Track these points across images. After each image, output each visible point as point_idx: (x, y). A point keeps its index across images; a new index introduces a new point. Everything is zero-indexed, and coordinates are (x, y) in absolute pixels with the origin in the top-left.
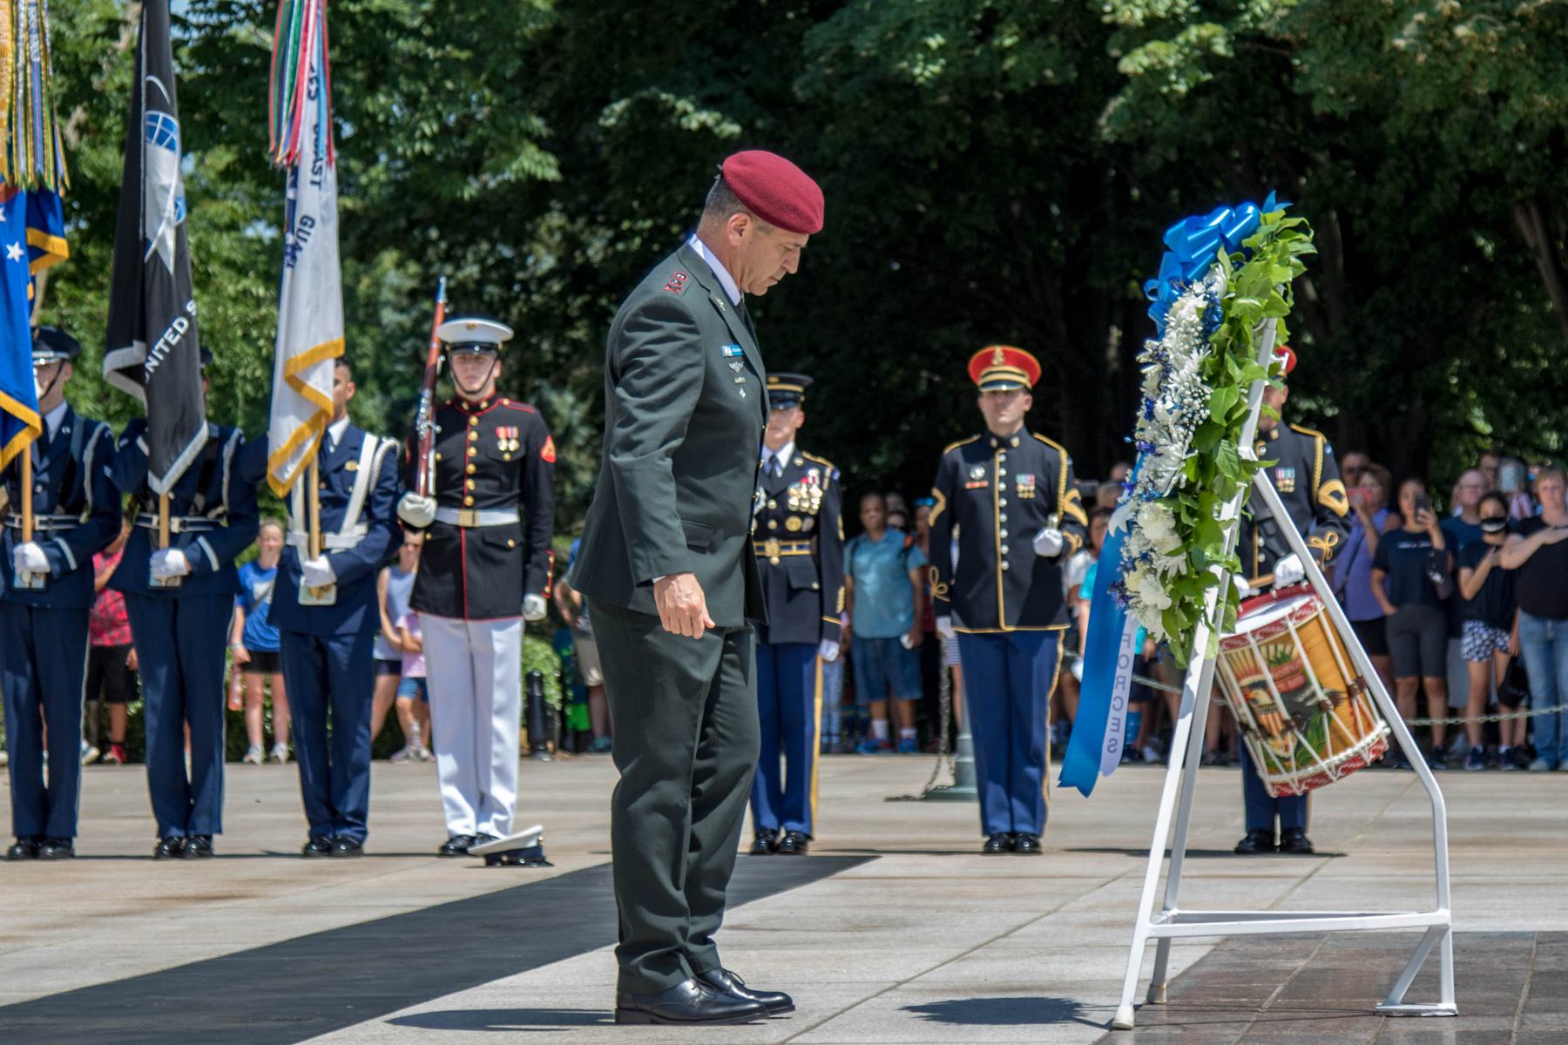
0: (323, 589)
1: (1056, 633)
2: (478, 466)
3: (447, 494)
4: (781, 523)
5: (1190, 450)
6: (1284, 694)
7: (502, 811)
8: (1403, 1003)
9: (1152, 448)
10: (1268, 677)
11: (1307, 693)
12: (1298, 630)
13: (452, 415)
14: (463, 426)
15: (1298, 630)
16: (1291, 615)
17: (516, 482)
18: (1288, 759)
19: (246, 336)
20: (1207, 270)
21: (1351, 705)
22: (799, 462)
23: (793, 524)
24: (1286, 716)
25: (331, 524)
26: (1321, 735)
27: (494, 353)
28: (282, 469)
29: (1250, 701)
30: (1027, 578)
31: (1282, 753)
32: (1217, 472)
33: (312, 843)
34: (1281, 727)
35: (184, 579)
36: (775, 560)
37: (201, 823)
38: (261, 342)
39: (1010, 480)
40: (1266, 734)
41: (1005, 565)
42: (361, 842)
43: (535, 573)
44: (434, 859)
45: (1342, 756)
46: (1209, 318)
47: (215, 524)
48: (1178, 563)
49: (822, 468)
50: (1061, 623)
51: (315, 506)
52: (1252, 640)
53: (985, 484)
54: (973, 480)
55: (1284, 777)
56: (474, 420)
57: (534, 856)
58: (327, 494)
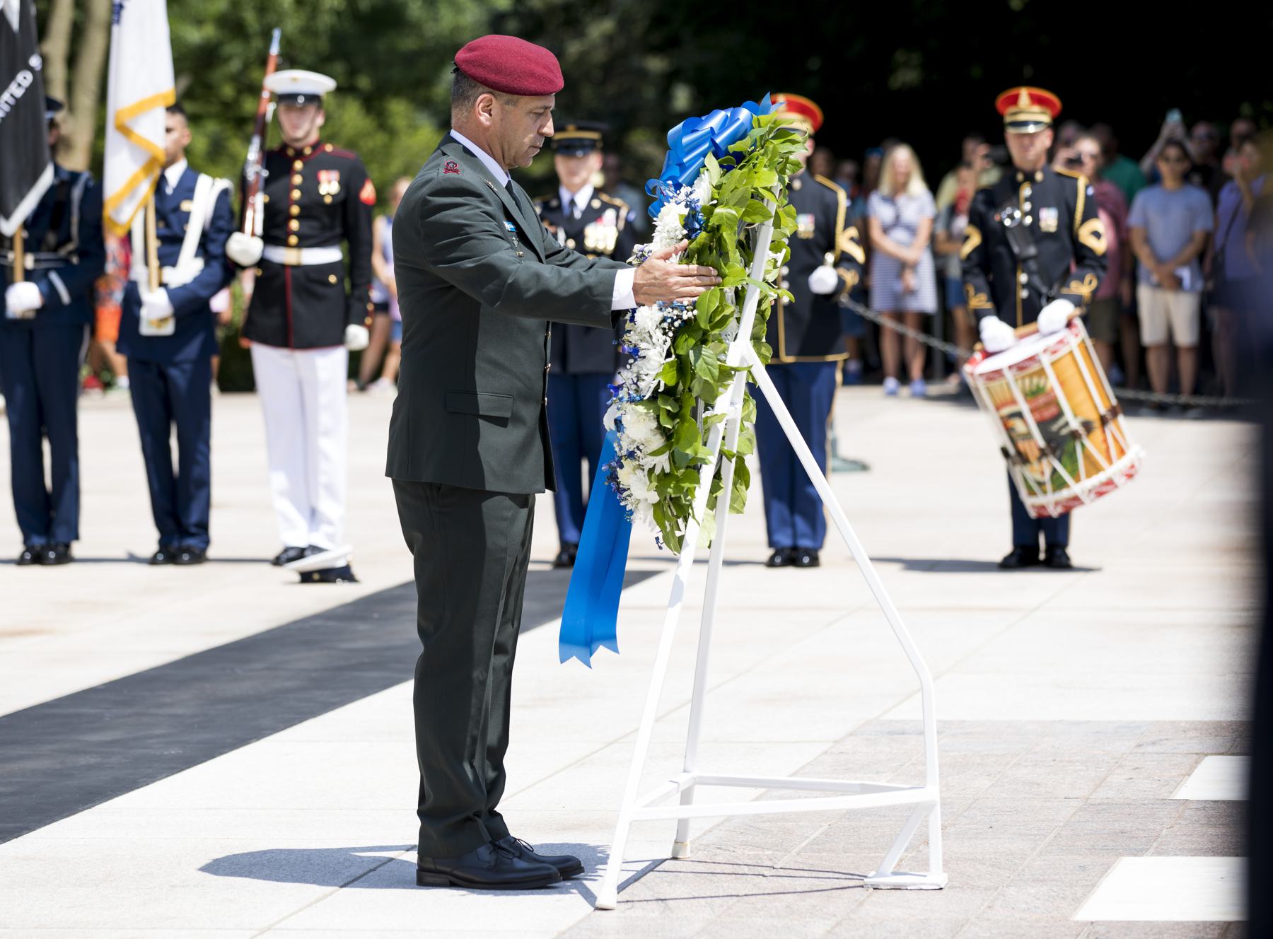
0: (163, 321)
1: (834, 363)
2: (302, 207)
3: (274, 233)
5: (668, 355)
7: (330, 523)
8: (895, 874)
9: (635, 351)
10: (1024, 407)
11: (1061, 422)
13: (279, 161)
14: (290, 171)
15: (1053, 364)
17: (338, 222)
20: (697, 174)
22: (596, 204)
24: (1041, 443)
25: (169, 257)
26: (1073, 455)
28: (118, 210)
30: (806, 313)
31: (1039, 477)
32: (694, 375)
33: (160, 552)
35: (39, 312)
37: (61, 533)
40: (1023, 459)
42: (204, 550)
43: (356, 306)
46: (690, 223)
47: (66, 261)
48: (663, 462)
49: (617, 209)
50: (839, 352)
51: (154, 244)
52: (1009, 375)
55: (1040, 500)
56: (298, 165)
57: (345, 574)
58: (165, 232)
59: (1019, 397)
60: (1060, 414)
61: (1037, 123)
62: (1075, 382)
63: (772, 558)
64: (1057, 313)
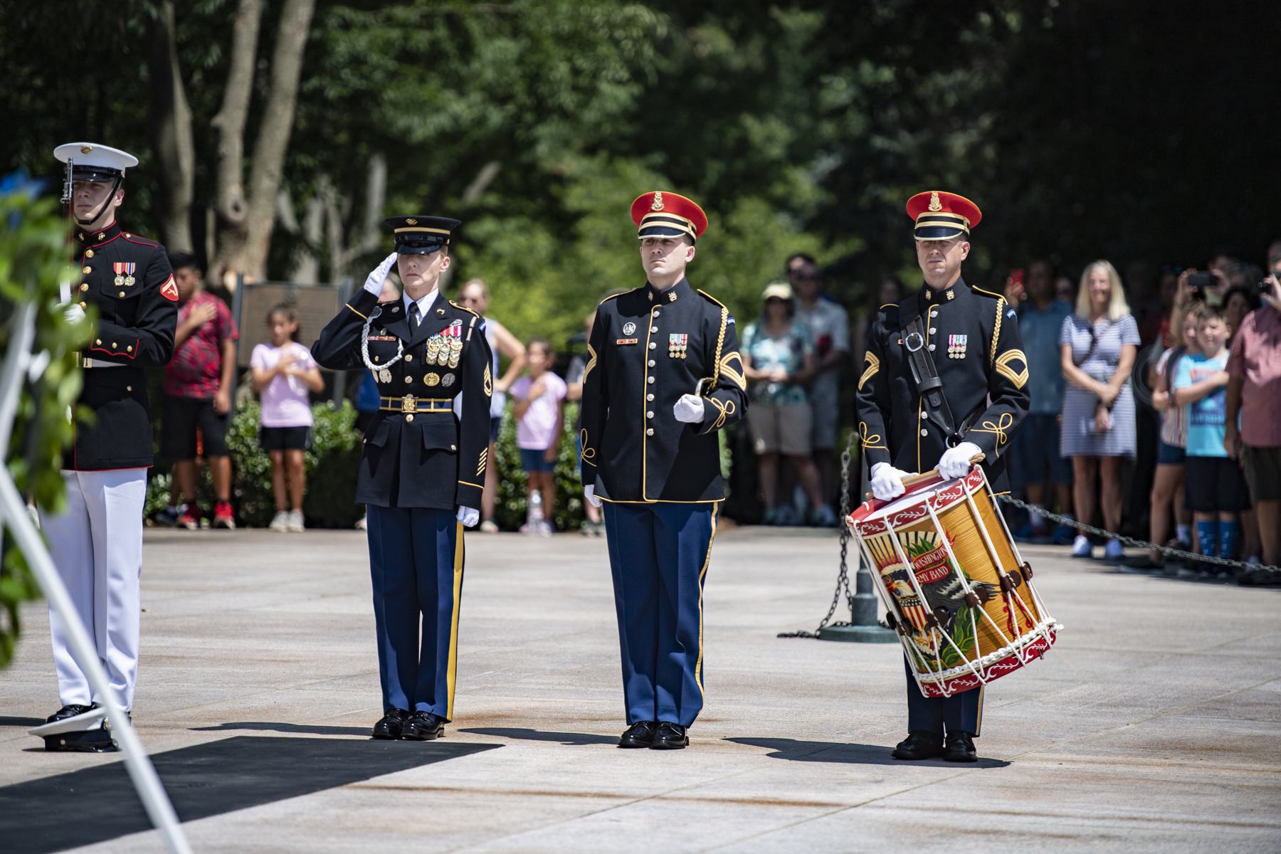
4: (418, 378)
6: (925, 586)
10: (909, 567)
11: (953, 585)
12: (940, 516)
16: (932, 500)
18: (934, 658)
21: (1006, 600)
23: (431, 380)
24: (929, 611)
27: (113, 181)
29: (893, 592)
31: (927, 650)
34: (925, 622)
36: (410, 418)
41: (651, 432)
44: (613, 749)
45: (993, 656)
53: (635, 341)
54: (624, 336)
60: (952, 575)
64: (961, 456)
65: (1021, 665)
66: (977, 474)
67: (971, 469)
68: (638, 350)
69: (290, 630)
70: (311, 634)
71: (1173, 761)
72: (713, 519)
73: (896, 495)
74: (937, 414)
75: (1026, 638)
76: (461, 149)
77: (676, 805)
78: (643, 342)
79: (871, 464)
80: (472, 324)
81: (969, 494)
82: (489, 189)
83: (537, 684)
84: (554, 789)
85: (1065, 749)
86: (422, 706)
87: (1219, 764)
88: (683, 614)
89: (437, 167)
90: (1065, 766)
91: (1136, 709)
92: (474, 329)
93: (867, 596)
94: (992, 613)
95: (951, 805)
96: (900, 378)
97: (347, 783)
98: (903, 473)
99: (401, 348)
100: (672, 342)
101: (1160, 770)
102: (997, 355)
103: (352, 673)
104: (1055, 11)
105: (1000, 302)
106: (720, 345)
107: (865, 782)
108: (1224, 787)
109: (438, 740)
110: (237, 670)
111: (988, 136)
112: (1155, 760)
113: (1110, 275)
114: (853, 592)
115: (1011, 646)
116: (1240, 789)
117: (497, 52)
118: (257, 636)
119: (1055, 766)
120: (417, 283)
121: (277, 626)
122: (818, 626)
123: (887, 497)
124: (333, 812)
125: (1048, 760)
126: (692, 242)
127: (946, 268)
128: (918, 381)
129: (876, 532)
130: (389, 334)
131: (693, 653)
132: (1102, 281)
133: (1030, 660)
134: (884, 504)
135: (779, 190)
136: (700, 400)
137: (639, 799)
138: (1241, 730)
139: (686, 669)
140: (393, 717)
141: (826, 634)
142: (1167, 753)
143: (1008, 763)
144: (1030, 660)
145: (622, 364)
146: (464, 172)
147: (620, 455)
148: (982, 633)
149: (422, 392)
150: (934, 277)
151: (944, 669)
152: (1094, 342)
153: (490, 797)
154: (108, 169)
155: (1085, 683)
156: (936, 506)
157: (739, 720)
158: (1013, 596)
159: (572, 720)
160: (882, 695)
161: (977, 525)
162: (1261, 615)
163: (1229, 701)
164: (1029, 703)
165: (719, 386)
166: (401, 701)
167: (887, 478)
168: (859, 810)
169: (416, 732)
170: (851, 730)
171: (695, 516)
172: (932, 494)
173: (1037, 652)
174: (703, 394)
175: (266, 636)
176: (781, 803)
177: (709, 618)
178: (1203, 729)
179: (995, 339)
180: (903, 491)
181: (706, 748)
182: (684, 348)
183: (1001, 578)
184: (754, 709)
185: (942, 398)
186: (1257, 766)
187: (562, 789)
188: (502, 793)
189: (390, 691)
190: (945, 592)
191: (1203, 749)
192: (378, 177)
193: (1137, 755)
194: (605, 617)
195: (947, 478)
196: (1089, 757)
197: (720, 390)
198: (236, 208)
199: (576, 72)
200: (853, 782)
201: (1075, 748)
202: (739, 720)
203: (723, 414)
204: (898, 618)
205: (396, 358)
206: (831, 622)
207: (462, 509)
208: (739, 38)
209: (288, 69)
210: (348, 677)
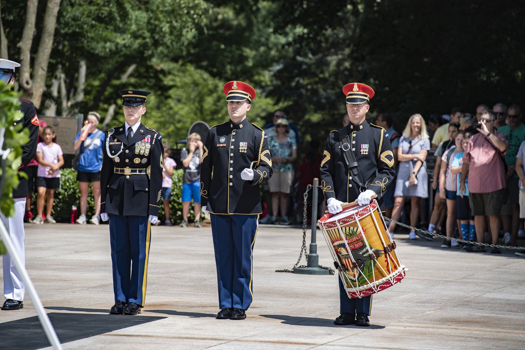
4: (131, 160)
6: (353, 250)
10: (346, 242)
11: (364, 250)
12: (360, 221)
16: (357, 213)
18: (355, 281)
19: (188, 13)
21: (386, 257)
23: (137, 161)
24: (354, 261)
31: (352, 278)
38: (195, 16)
39: (237, 146)
41: (231, 184)
44: (214, 319)
45: (380, 281)
52: (338, 224)
53: (225, 145)
54: (220, 143)
59: (343, 236)
60: (364, 246)
61: (363, 100)
62: (372, 231)
63: (219, 313)
64: (367, 196)
65: (392, 285)
66: (374, 203)
67: (371, 202)
68: (226, 150)
69: (65, 267)
70: (75, 269)
71: (453, 327)
72: (257, 221)
73: (338, 212)
74: (356, 178)
75: (394, 273)
76: (117, 59)
77: (246, 343)
78: (228, 145)
79: (327, 199)
80: (155, 137)
81: (372, 211)
82: (131, 75)
83: (176, 291)
84: (192, 336)
85: (406, 321)
86: (131, 300)
87: (472, 328)
88: (244, 262)
89: (109, 66)
90: (407, 328)
91: (432, 304)
92: (156, 139)
93: (314, 255)
94: (381, 262)
95: (362, 345)
96: (340, 162)
97: (100, 334)
98: (341, 203)
99: (122, 147)
100: (241, 146)
101: (447, 330)
102: (381, 153)
103: (95, 285)
104: (379, 4)
105: (382, 130)
106: (261, 147)
107: (324, 334)
108: (476, 338)
109: (138, 315)
110: (45, 284)
111: (350, 56)
112: (445, 326)
113: (420, 119)
114: (308, 252)
115: (388, 277)
116: (483, 339)
117: (138, 16)
118: (51, 269)
119: (403, 328)
120: (133, 118)
121: (59, 265)
122: (293, 267)
123: (334, 213)
124: (99, 345)
125: (399, 326)
126: (249, 102)
127: (360, 116)
128: (348, 164)
129: (332, 227)
130: (118, 141)
131: (248, 277)
132: (417, 123)
133: (396, 283)
134: (332, 216)
135: (256, 78)
136: (252, 171)
137: (229, 341)
138: (478, 314)
139: (245, 285)
140: (118, 304)
141: (297, 271)
142: (449, 323)
143: (384, 327)
144: (396, 283)
145: (219, 155)
146: (121, 68)
147: (218, 194)
148: (376, 271)
149: (133, 166)
150: (354, 119)
151: (359, 286)
152: (411, 147)
153: (166, 339)
154: (8, 69)
155: (409, 293)
156: (358, 216)
157: (266, 307)
158: (389, 255)
159: (192, 307)
160: (324, 297)
161: (375, 225)
162: (478, 265)
163: (471, 301)
164: (387, 301)
165: (260, 165)
166: (122, 298)
167: (334, 204)
168: (324, 346)
169: (129, 311)
170: (314, 312)
171: (249, 220)
172: (357, 211)
173: (399, 278)
174: (253, 168)
175: (55, 269)
176: (290, 343)
177: (255, 264)
178: (464, 313)
179: (380, 146)
180: (341, 210)
181: (254, 319)
182: (246, 148)
183: (384, 248)
184: (271, 303)
185: (358, 171)
186: (488, 329)
187: (196, 336)
188: (170, 338)
189: (118, 293)
190: (361, 253)
191: (464, 322)
192: (83, 70)
193: (437, 324)
194: (210, 262)
195: (361, 205)
196: (417, 325)
197: (261, 166)
198: (27, 83)
199: (172, 28)
200: (319, 334)
201: (410, 321)
202: (266, 307)
203: (262, 176)
204: (340, 264)
205: (120, 152)
206: (298, 266)
207: (150, 216)
208: (237, 13)
209: (51, 24)
210: (94, 287)
